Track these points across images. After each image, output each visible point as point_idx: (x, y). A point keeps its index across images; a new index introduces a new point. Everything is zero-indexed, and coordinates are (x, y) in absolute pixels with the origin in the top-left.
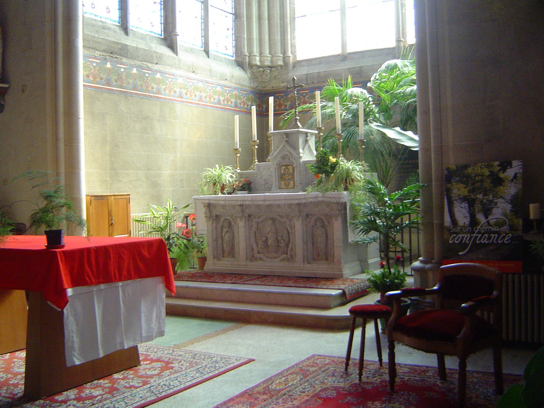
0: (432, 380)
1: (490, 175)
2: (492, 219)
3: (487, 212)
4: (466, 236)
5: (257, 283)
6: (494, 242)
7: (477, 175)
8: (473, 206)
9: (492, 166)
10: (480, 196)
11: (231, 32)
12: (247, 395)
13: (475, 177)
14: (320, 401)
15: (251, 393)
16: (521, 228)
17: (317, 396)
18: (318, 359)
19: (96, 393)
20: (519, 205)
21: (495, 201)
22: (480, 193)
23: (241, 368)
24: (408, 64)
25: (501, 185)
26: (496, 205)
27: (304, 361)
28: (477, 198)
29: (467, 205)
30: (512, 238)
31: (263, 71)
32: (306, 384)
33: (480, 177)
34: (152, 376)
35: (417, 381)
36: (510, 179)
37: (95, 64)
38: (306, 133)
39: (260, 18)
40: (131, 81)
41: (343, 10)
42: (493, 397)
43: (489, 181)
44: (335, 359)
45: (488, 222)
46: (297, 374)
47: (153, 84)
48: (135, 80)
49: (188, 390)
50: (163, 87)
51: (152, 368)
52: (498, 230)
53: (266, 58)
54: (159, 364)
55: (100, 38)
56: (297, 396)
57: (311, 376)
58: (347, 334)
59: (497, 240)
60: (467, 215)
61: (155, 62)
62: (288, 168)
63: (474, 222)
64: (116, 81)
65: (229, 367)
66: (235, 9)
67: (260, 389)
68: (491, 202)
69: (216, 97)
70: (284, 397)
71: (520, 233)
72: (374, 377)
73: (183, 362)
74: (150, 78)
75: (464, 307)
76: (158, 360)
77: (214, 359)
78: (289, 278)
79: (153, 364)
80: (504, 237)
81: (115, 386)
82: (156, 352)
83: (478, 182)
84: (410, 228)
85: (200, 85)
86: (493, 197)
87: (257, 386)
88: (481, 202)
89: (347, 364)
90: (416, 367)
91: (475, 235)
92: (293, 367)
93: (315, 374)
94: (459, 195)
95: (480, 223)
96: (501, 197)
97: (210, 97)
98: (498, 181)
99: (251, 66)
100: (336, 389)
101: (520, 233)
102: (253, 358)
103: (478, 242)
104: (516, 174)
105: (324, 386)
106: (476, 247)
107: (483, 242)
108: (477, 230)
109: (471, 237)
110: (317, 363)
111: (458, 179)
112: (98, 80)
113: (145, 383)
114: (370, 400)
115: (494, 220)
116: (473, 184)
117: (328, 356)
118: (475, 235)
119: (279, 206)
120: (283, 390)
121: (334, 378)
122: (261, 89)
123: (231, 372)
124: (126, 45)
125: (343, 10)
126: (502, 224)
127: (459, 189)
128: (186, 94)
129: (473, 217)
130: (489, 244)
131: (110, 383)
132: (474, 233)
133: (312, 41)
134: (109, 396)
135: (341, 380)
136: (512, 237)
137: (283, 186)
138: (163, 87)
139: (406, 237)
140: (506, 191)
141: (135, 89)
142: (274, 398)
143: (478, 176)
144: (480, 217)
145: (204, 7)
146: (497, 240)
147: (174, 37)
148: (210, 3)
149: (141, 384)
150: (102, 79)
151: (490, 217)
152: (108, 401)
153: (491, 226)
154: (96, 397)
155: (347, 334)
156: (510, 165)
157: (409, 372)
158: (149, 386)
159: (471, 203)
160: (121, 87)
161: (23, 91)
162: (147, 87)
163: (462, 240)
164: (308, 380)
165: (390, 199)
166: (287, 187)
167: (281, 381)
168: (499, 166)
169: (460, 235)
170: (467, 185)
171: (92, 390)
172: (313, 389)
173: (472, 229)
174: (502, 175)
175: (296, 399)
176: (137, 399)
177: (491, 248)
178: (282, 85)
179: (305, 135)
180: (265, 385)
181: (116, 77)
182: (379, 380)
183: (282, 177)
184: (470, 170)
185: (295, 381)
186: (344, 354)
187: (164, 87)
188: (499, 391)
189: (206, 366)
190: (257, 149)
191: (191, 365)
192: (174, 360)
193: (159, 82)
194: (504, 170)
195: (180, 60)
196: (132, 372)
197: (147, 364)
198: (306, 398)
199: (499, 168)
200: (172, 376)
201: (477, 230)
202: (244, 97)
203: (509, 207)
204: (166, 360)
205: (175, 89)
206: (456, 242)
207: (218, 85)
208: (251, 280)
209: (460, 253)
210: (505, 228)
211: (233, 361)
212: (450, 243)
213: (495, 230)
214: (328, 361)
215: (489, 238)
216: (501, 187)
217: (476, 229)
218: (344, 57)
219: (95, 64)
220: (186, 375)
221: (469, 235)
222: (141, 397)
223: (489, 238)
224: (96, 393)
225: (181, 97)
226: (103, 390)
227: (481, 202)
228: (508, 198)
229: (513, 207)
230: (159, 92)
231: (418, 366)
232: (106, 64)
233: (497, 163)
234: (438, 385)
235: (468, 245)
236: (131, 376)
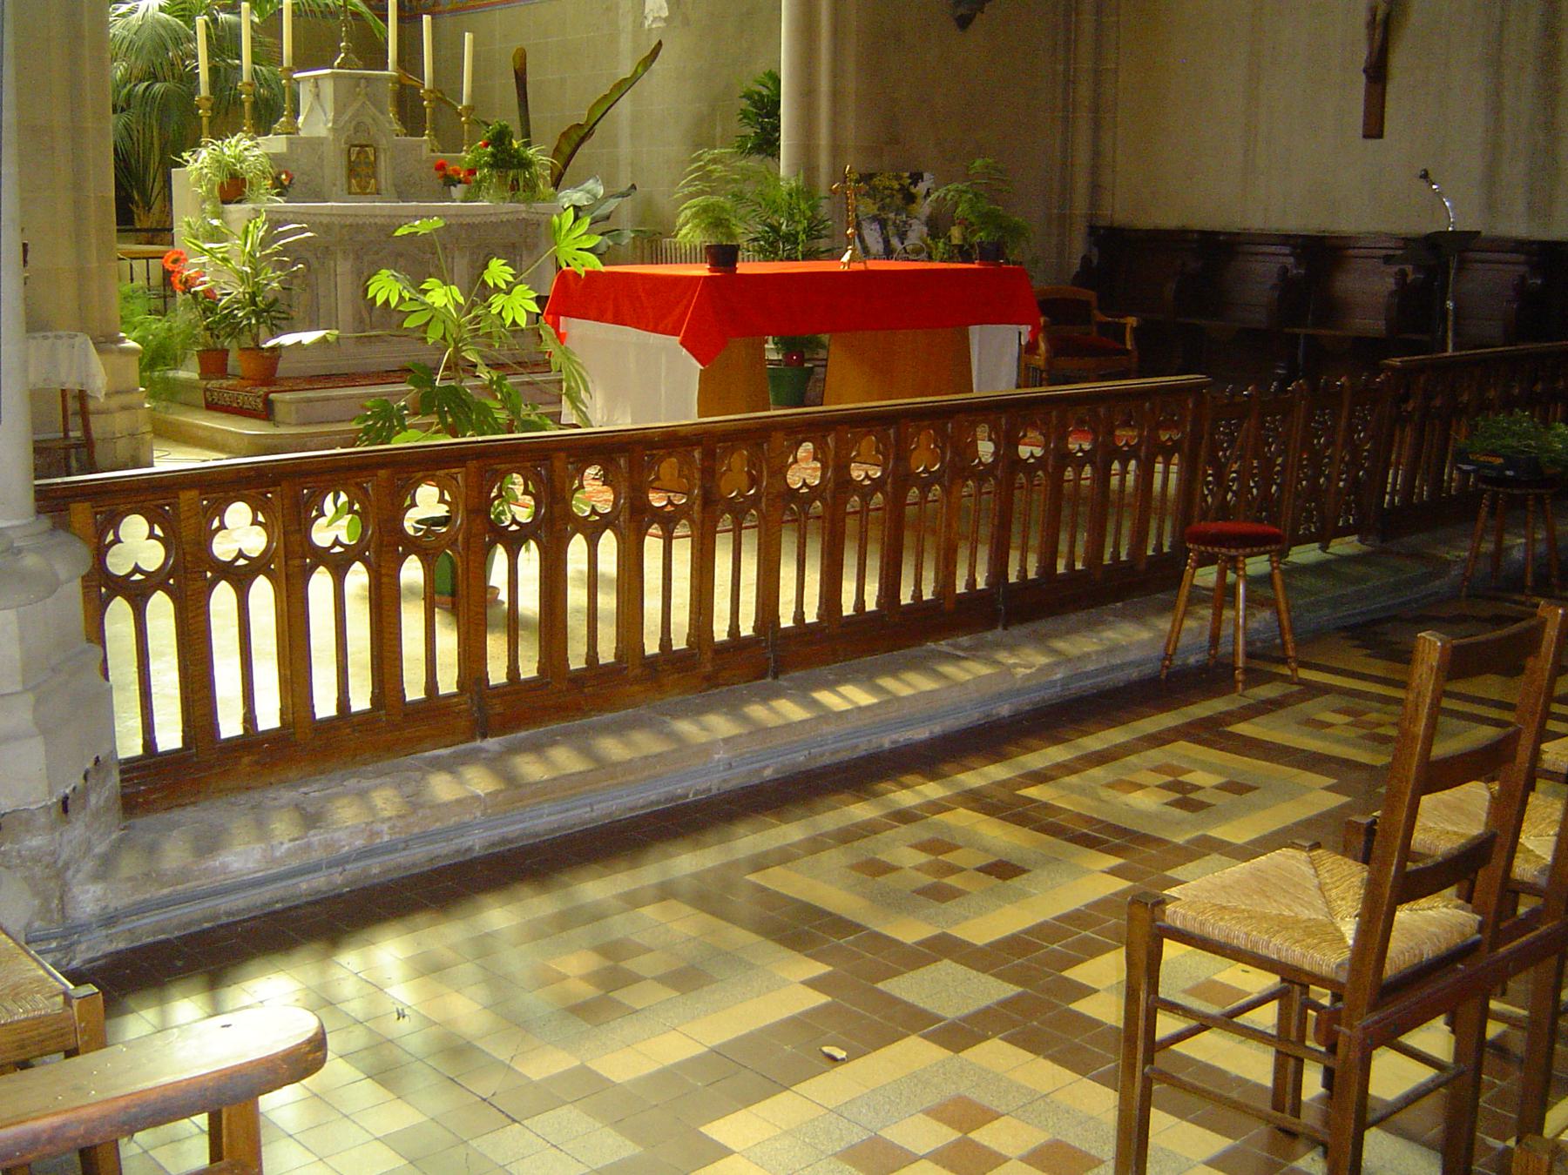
3: (902, 237)
10: (892, 216)
78: (366, 375)
98: (910, 198)
129: (887, 242)
137: (355, 188)
144: (895, 242)
159: (883, 224)
166: (363, 192)
174: (913, 190)
183: (352, 170)
190: (1134, 330)
194: (915, 184)
203: (925, 229)
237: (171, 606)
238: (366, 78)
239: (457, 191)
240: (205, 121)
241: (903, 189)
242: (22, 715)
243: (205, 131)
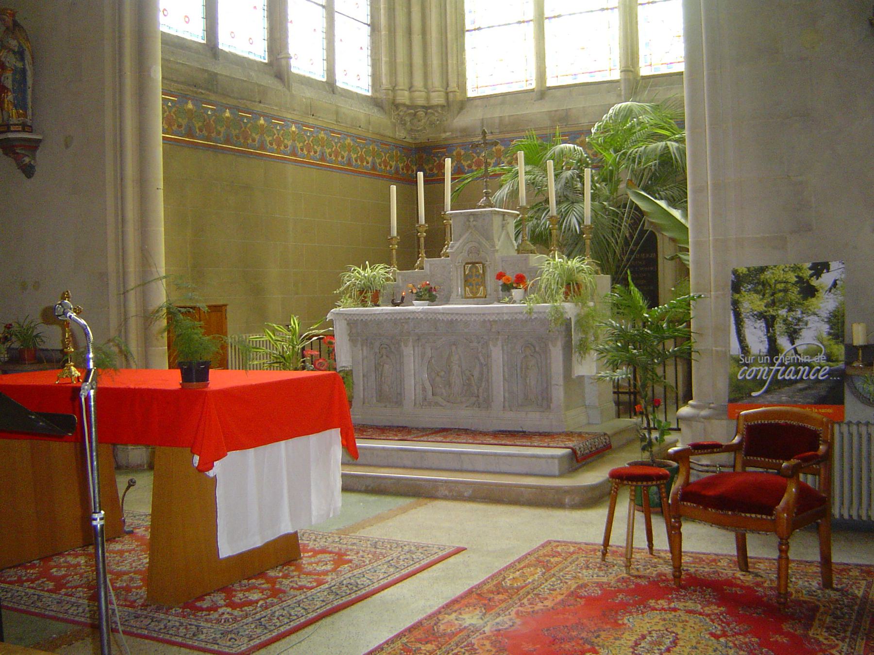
0: (730, 573)
1: (797, 282)
2: (801, 344)
3: (793, 335)
4: (762, 369)
5: (439, 439)
6: (804, 378)
7: (777, 282)
8: (772, 326)
9: (800, 269)
10: (783, 312)
11: (367, 52)
12: (474, 595)
13: (775, 284)
14: (582, 602)
15: (478, 592)
16: (842, 357)
17: (574, 594)
18: (558, 546)
19: (255, 596)
20: (838, 325)
21: (805, 319)
22: (783, 308)
23: (452, 560)
24: (648, 109)
25: (813, 296)
26: (806, 325)
27: (537, 550)
28: (778, 315)
29: (764, 325)
30: (830, 373)
31: (415, 115)
32: (553, 579)
33: (783, 285)
34: (326, 573)
35: (709, 573)
36: (827, 288)
37: (170, 104)
38: (504, 214)
39: (409, 32)
40: (222, 130)
41: (540, 20)
42: (819, 591)
43: (796, 290)
44: (583, 546)
45: (795, 349)
46: (535, 566)
47: (254, 135)
48: (228, 127)
49: (386, 591)
50: (268, 139)
51: (320, 561)
52: (809, 360)
53: (417, 94)
54: (327, 557)
55: (177, 63)
56: (546, 596)
57: (557, 569)
58: (603, 512)
59: (808, 375)
60: (765, 339)
61: (257, 100)
62: (477, 268)
63: (773, 350)
64: (201, 130)
65: (432, 558)
66: (372, 17)
67: (491, 586)
68: (799, 320)
69: (345, 154)
70: (529, 597)
71: (841, 365)
72: (645, 570)
73: (361, 553)
74: (249, 125)
75: (785, 467)
76: (323, 551)
77: (406, 548)
78: (485, 434)
79: (319, 556)
80: (818, 371)
81: (277, 586)
82: (315, 540)
83: (780, 291)
84: (676, 357)
85: (322, 135)
86: (802, 313)
87: (484, 583)
88: (785, 320)
89: (604, 554)
90: (701, 556)
91: (775, 368)
92: (525, 557)
93: (561, 566)
94: (752, 310)
95: (783, 350)
96: (815, 314)
97: (337, 154)
98: (809, 291)
99: (396, 106)
100: (599, 585)
101: (841, 365)
102: (466, 546)
103: (779, 378)
104: (835, 281)
105: (580, 582)
106: (777, 384)
107: (787, 378)
108: (779, 361)
109: (770, 371)
110: (558, 552)
111: (750, 287)
112: (175, 128)
113: (320, 583)
114: (652, 598)
115: (805, 347)
116: (773, 294)
117: (571, 543)
118: (775, 368)
119: (466, 324)
120: (523, 587)
121: (591, 572)
122: (411, 141)
123: (439, 565)
124: (216, 74)
125: (540, 20)
126: (814, 353)
127: (752, 302)
128: (302, 150)
130: (796, 382)
131: (267, 583)
132: (773, 364)
133: (494, 65)
134: (275, 600)
135: (601, 574)
136: (830, 370)
138: (268, 139)
139: (670, 370)
140: (821, 305)
141: (227, 142)
142: (515, 598)
143: (780, 282)
144: (783, 342)
145: (327, 14)
146: (808, 375)
147: (283, 62)
148: (337, 7)
149: (315, 584)
150: (180, 126)
151: (798, 342)
152: (277, 607)
153: (800, 355)
154: (257, 602)
155: (603, 512)
156: (825, 266)
157: (693, 562)
158: (327, 586)
159: (770, 322)
160: (208, 139)
161: (67, 146)
162: (246, 139)
163: (756, 375)
164: (554, 575)
165: (651, 316)
166: (474, 297)
167: (515, 576)
168: (810, 269)
169: (754, 368)
170: (764, 295)
171: (247, 594)
172: (566, 586)
173: (772, 360)
174: (814, 282)
175: (546, 599)
176: (319, 604)
177: (800, 386)
178: (444, 136)
179: (501, 218)
180: (495, 582)
181: (200, 124)
182: (655, 573)
183: (467, 280)
184: (767, 275)
185: (536, 576)
186: (600, 540)
187: (270, 138)
188: (827, 584)
189: (398, 558)
191: (376, 557)
192: (347, 550)
193: (262, 130)
195: (292, 96)
196: (292, 568)
197: (309, 557)
198: (560, 598)
199: (811, 272)
200: (355, 572)
201: (779, 361)
202: (385, 154)
203: (825, 328)
204: (337, 550)
205: (286, 141)
206: (748, 378)
207: (348, 136)
208: (423, 436)
209: (754, 394)
210: (820, 358)
211: (435, 550)
212: (738, 380)
213: (805, 360)
214: (572, 549)
215: (797, 372)
216: (814, 299)
217: (777, 359)
218: (543, 93)
219: (170, 104)
220: (375, 571)
221: (766, 368)
222: (323, 601)
223: (797, 372)
224: (255, 596)
225: (294, 153)
226: (262, 592)
227: (785, 320)
228: (825, 314)
229: (831, 328)
230: (262, 147)
231: (704, 554)
232: (187, 103)
233: (809, 265)
234: (739, 579)
235: (766, 381)
236: (295, 573)
237: (232, 455)
238: (472, 214)
239: (516, 293)
240: (422, 240)
241: (800, 279)
242: (243, 37)
243: (423, 251)
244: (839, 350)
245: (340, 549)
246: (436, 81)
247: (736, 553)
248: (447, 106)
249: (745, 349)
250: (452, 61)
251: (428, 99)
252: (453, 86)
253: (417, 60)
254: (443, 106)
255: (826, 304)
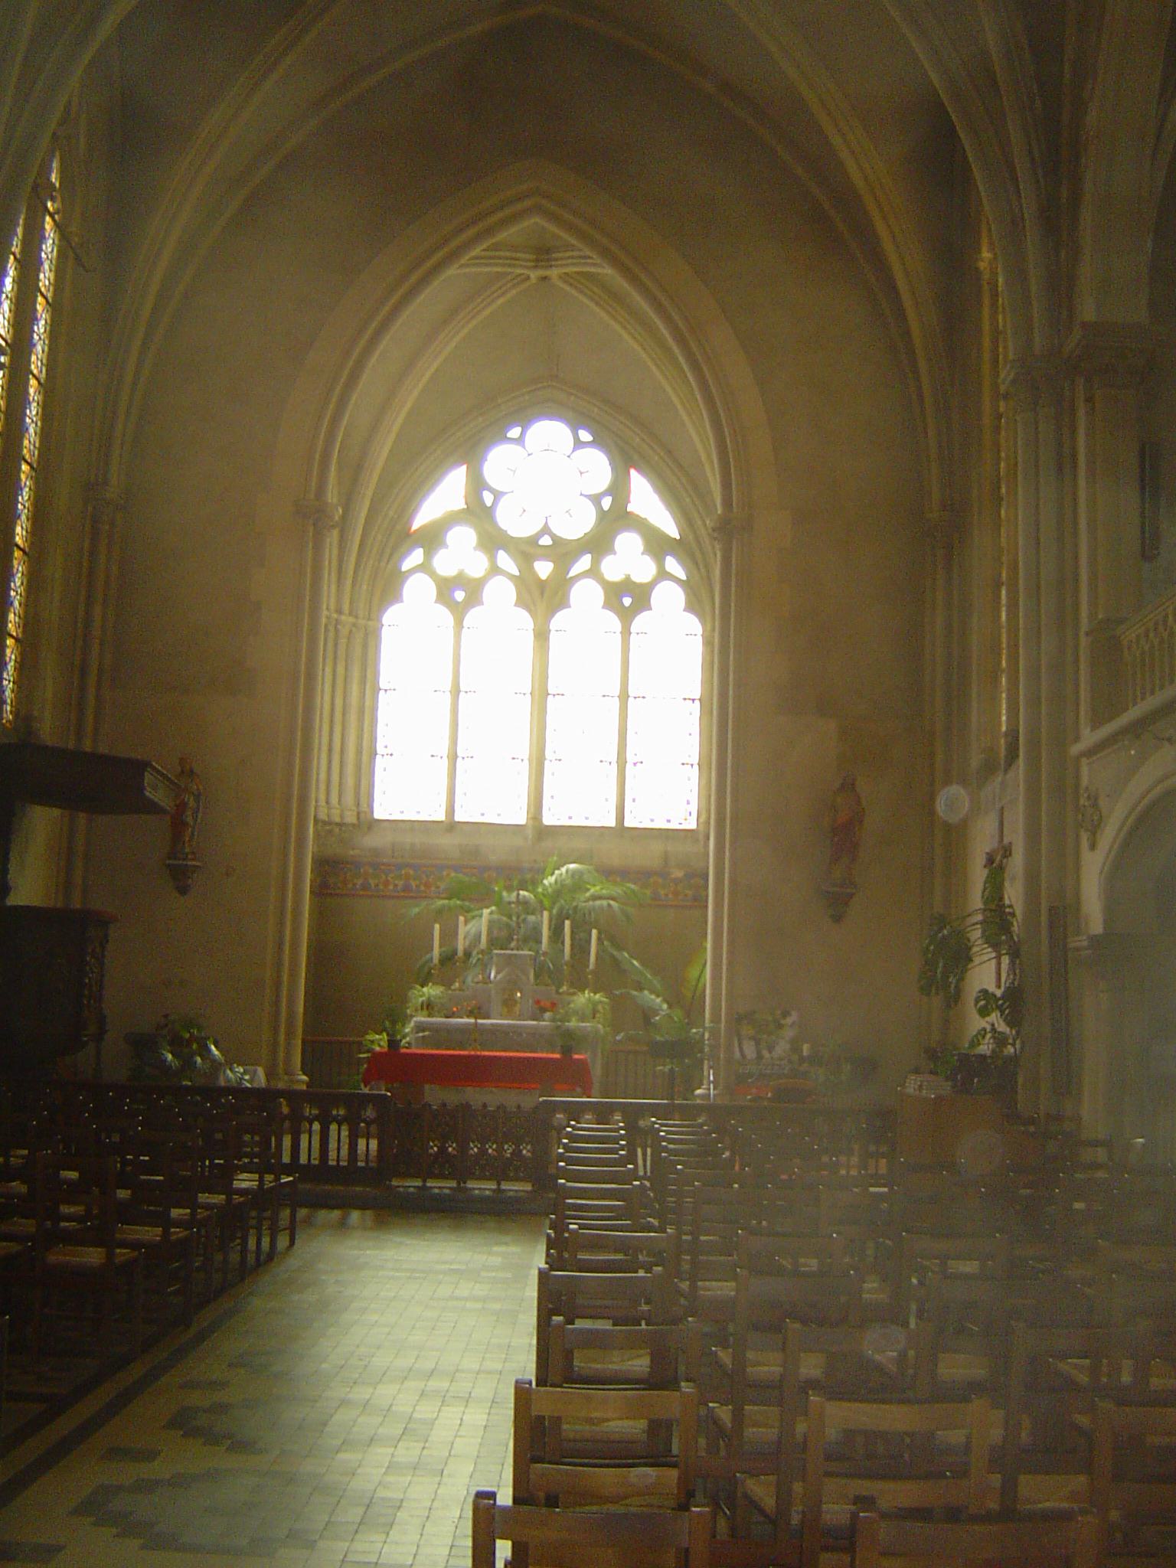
3: (770, 1049)
20: (795, 1048)
63: (760, 1057)
98: (780, 1026)
126: (781, 1059)
127: (747, 1030)
144: (766, 1054)
159: (758, 1042)
203: (788, 1046)
244: (795, 1057)
245: (485, 1106)
246: (349, 798)
247: (56, 812)
248: (356, 826)
249: (743, 1055)
250: (364, 782)
251: (342, 816)
252: (364, 807)
253: (335, 777)
254: (353, 825)
255: (789, 1033)
